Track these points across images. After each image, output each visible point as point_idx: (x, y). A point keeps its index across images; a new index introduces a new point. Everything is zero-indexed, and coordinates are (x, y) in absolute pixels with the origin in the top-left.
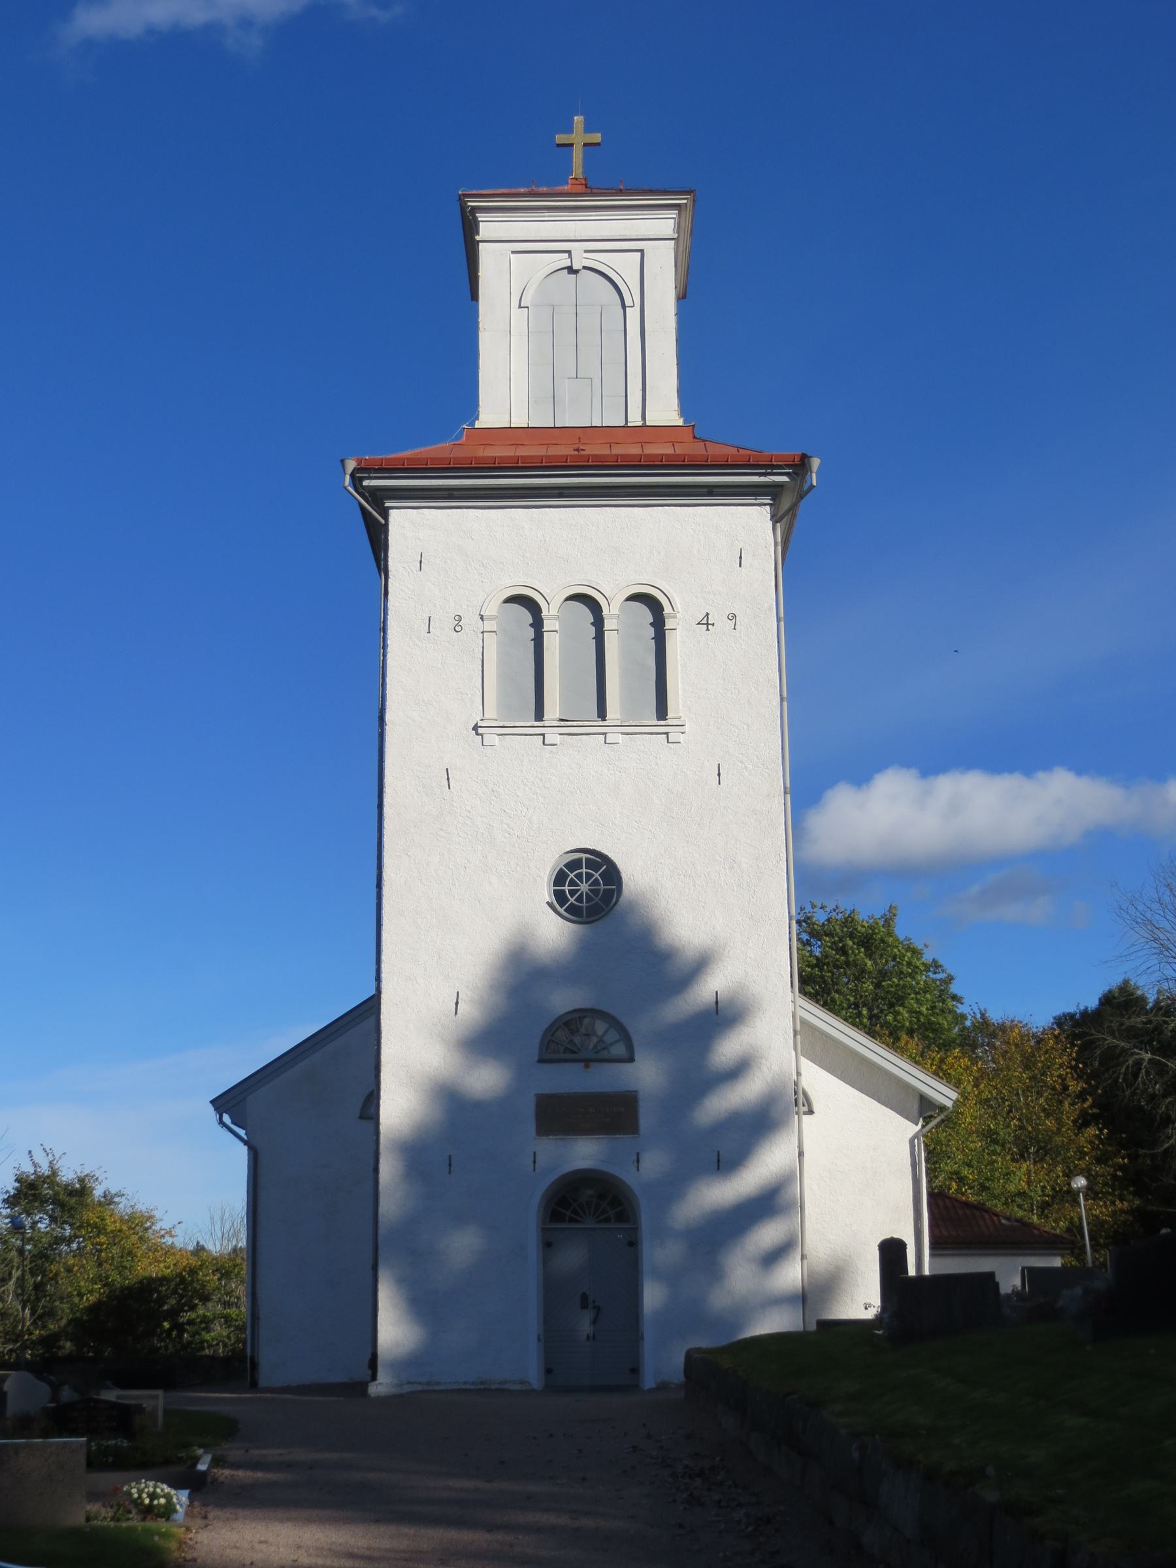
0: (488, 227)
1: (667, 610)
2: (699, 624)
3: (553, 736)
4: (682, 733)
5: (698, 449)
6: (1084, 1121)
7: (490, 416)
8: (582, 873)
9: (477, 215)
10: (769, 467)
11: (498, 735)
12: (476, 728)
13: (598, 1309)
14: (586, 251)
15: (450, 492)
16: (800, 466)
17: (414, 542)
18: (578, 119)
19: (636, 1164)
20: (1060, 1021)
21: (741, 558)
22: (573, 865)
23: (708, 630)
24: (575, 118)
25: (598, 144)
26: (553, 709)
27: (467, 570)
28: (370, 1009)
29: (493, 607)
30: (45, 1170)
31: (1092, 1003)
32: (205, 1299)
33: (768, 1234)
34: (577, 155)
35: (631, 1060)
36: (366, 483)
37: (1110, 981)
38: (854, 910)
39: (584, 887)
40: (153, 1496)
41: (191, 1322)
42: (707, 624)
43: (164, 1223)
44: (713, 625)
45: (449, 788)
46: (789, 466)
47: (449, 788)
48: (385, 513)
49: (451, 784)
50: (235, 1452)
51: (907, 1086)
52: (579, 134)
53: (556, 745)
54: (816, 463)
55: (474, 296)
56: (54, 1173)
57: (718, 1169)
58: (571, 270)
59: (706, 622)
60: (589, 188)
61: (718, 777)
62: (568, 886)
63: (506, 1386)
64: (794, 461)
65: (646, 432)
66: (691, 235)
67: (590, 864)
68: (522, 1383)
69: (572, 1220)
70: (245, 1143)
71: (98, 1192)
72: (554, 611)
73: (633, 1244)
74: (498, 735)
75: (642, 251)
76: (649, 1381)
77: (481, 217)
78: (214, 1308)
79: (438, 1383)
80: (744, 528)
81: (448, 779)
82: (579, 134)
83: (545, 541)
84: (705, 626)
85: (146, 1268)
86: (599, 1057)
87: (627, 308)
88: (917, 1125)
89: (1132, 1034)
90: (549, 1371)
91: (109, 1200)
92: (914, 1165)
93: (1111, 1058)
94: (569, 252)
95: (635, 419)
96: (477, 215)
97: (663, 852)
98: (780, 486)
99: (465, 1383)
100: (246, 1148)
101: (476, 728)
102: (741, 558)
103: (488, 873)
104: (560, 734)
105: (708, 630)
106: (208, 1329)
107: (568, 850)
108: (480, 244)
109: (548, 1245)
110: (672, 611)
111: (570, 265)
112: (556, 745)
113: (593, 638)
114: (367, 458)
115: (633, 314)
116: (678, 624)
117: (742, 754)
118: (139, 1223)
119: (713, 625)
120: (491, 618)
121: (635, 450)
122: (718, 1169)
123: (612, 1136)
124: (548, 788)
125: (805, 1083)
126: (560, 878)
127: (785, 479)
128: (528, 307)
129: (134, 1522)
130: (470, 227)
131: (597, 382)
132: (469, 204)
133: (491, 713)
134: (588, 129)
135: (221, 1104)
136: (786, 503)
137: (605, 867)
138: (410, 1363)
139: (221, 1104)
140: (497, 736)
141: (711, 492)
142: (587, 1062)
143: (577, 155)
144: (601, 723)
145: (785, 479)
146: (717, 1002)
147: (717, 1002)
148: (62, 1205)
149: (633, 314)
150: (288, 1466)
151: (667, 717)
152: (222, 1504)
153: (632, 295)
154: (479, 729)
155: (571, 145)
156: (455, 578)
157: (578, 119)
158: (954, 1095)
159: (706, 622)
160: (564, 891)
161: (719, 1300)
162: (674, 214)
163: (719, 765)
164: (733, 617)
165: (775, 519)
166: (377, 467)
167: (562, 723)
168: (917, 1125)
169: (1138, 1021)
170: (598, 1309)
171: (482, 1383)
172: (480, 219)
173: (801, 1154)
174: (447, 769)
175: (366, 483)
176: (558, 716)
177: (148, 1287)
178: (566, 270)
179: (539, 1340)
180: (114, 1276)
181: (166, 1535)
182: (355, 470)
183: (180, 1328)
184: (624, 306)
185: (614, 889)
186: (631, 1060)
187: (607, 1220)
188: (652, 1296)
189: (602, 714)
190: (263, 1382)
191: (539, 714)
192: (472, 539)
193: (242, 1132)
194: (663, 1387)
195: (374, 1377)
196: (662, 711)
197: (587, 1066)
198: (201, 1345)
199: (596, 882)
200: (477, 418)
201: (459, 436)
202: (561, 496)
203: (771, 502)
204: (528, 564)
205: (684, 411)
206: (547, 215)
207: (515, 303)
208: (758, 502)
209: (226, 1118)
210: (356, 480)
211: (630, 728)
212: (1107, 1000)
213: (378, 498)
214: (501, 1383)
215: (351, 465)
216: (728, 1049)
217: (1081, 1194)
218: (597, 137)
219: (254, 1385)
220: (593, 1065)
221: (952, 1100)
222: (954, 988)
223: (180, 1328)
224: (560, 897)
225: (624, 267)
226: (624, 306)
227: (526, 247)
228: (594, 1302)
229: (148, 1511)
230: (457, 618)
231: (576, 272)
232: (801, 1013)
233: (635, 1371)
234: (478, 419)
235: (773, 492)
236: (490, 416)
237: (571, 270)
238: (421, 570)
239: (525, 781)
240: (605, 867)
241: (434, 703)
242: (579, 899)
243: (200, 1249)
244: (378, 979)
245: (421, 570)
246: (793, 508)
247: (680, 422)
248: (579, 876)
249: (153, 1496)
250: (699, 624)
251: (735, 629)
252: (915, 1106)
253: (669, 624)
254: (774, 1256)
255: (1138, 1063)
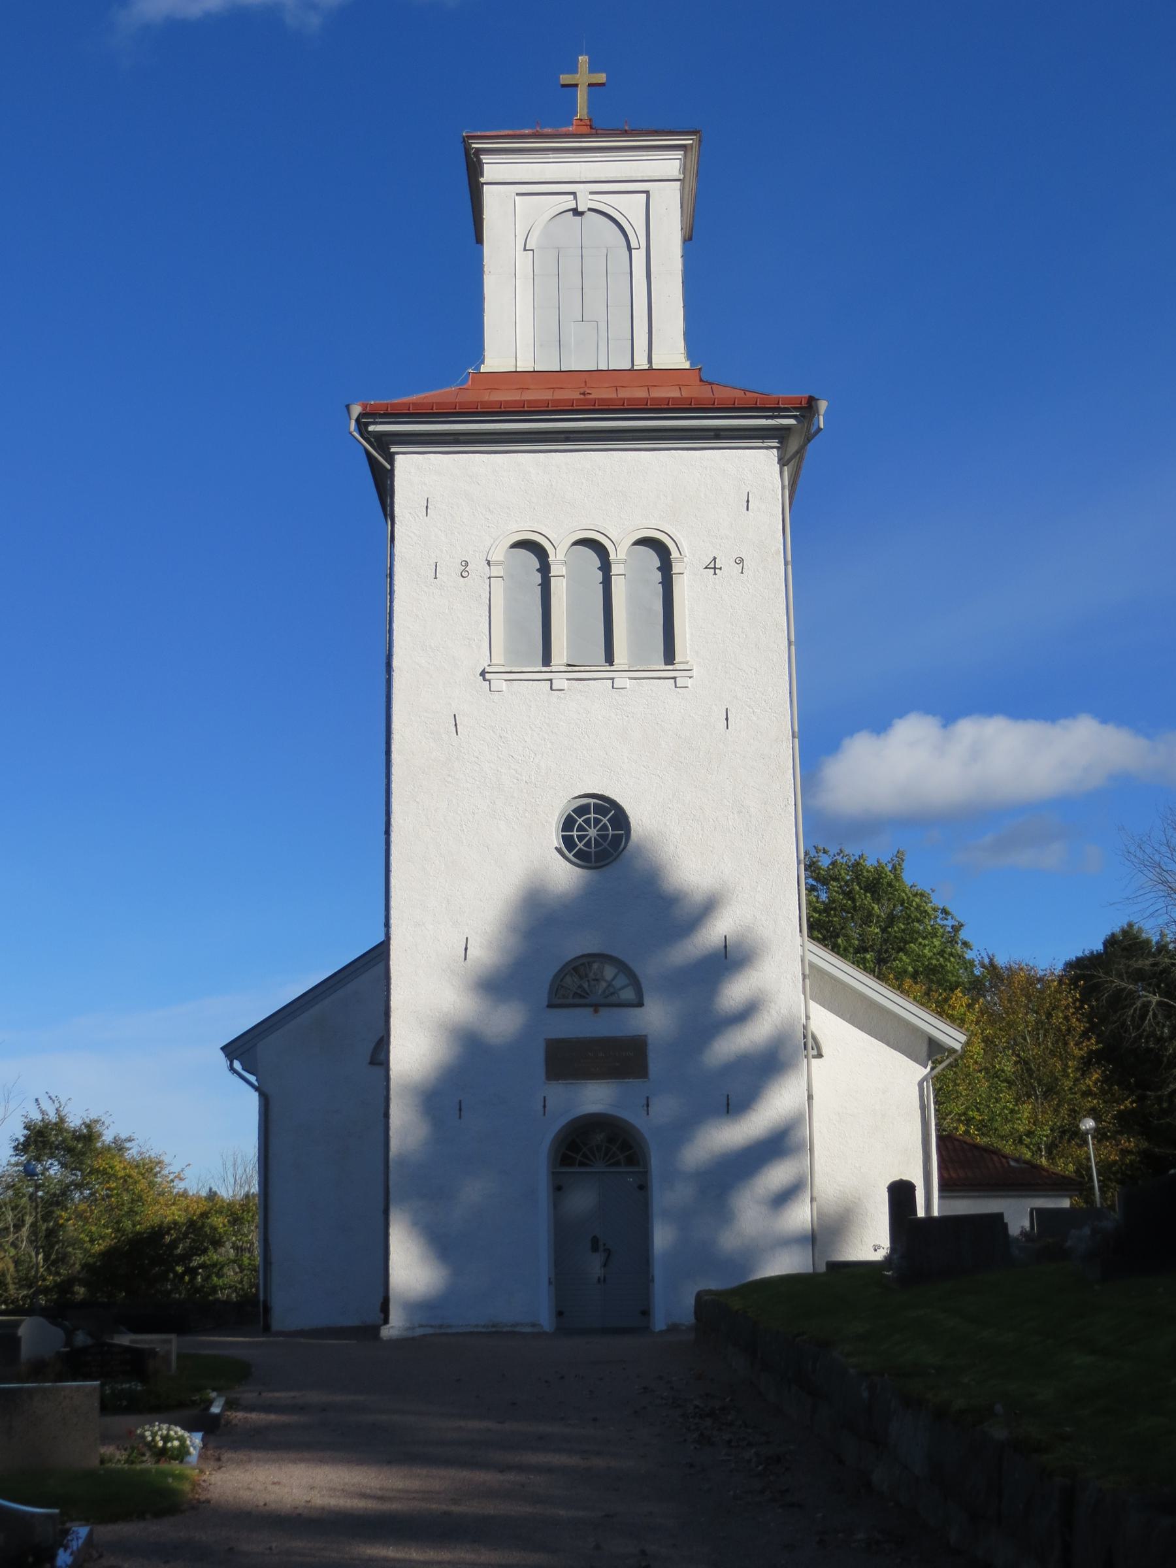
0: (493, 169)
1: (674, 554)
2: (706, 568)
3: (560, 682)
4: (690, 678)
5: (704, 393)
6: (1086, 1065)
7: (495, 360)
8: (590, 818)
9: (481, 157)
10: (776, 410)
11: (506, 680)
12: (483, 674)
13: (609, 1252)
14: (591, 193)
15: (456, 437)
16: (807, 409)
17: (420, 488)
18: (583, 59)
19: (645, 1108)
20: (1069, 965)
21: (748, 501)
22: (582, 810)
23: (715, 574)
24: (580, 58)
25: (603, 85)
26: (560, 654)
27: (474, 515)
28: (379, 955)
29: (499, 553)
30: (53, 1117)
31: (1099, 947)
32: (217, 1243)
33: (777, 1175)
34: (582, 95)
35: (640, 1004)
36: (371, 428)
37: (1113, 925)
38: (862, 854)
39: (592, 832)
40: (166, 1439)
41: (203, 1266)
42: (715, 568)
43: (173, 1166)
44: (720, 569)
45: (457, 734)
46: (796, 409)
47: (457, 734)
48: (391, 459)
49: (458, 730)
50: (248, 1395)
51: (916, 1030)
52: (583, 74)
53: (563, 690)
54: (823, 406)
55: (479, 239)
56: (62, 1120)
57: (725, 937)
58: (576, 212)
59: (713, 567)
60: (594, 129)
61: (725, 722)
62: (577, 832)
63: (517, 1329)
64: (801, 404)
65: (652, 374)
66: (697, 176)
67: (599, 809)
68: (534, 1325)
69: (582, 1164)
70: (256, 1089)
71: (108, 1137)
72: (561, 555)
73: (643, 1187)
74: (506, 680)
75: (647, 192)
76: (659, 1323)
77: (485, 159)
78: (228, 1251)
79: (449, 1326)
80: (751, 471)
81: (456, 725)
82: (583, 74)
83: (552, 485)
84: (713, 570)
85: (155, 1214)
86: (610, 1002)
87: (633, 251)
88: (926, 1067)
89: (1139, 976)
90: (560, 1314)
91: (119, 1146)
92: (923, 1108)
93: (1119, 1000)
94: (574, 194)
95: (641, 363)
96: (481, 157)
97: (671, 797)
98: (787, 429)
99: (477, 1326)
100: (256, 1094)
101: (483, 674)
102: (748, 501)
103: (496, 818)
104: (568, 679)
105: (715, 574)
106: (220, 1275)
107: (577, 795)
108: (485, 186)
109: (558, 1188)
110: (679, 556)
111: (575, 206)
112: (563, 690)
113: (600, 583)
114: (372, 403)
115: (639, 257)
116: (686, 568)
117: (750, 699)
118: (149, 1168)
119: (720, 569)
120: (498, 563)
121: (641, 393)
122: (725, 937)
123: (621, 1081)
124: (556, 733)
125: (814, 1026)
126: (568, 824)
127: (792, 422)
128: (533, 250)
129: (148, 1463)
130: (474, 169)
131: (603, 326)
132: (473, 146)
133: (498, 658)
134: (593, 69)
135: (232, 1050)
136: (793, 445)
137: (613, 812)
138: (424, 1307)
139: (232, 1050)
140: (504, 682)
141: (717, 435)
142: (596, 1007)
143: (582, 95)
144: (609, 668)
145: (792, 422)
146: (726, 947)
147: (726, 947)
148: (70, 1150)
149: (639, 257)
150: (301, 1409)
151: (675, 662)
152: (235, 1446)
153: (638, 238)
154: (486, 674)
155: (576, 85)
156: (462, 523)
157: (583, 59)
158: (963, 1039)
159: (713, 567)
160: (573, 836)
161: (729, 1241)
162: (679, 154)
163: (727, 709)
164: (740, 561)
165: (782, 462)
166: (382, 412)
167: (570, 669)
168: (926, 1067)
169: (1145, 963)
170: (609, 1252)
171: (493, 1326)
172: (484, 161)
173: (810, 1097)
174: (455, 715)
175: (371, 428)
176: (565, 661)
177: (157, 1233)
178: (571, 212)
179: (550, 1283)
180: (127, 1224)
181: (181, 1477)
182: (361, 415)
183: (193, 1272)
184: (629, 248)
185: (622, 834)
186: (640, 1004)
187: (617, 1164)
188: (662, 1237)
189: (610, 659)
190: (276, 1325)
191: (547, 660)
192: (479, 484)
193: (252, 1079)
194: (673, 1329)
195: (386, 1321)
196: (669, 656)
197: (596, 1011)
198: (214, 1289)
199: (604, 828)
200: (483, 362)
201: (465, 381)
202: (567, 440)
203: (779, 445)
204: (535, 509)
205: (690, 354)
206: (552, 157)
207: (520, 246)
208: (765, 445)
209: (237, 1065)
210: (361, 426)
211: (637, 673)
212: (1111, 942)
213: (384, 443)
214: (512, 1326)
215: (356, 410)
216: (736, 992)
217: (1090, 1136)
218: (601, 78)
219: (267, 1329)
220: (604, 1012)
221: (961, 1043)
222: (963, 935)
223: (193, 1272)
224: (568, 842)
225: (630, 208)
226: (629, 248)
227: (530, 189)
228: (604, 1245)
229: (162, 1454)
230: (463, 563)
231: (581, 214)
232: (810, 957)
233: (646, 1313)
234: (483, 363)
235: (780, 435)
236: (495, 360)
237: (576, 212)
238: (427, 515)
239: (533, 726)
240: (613, 812)
241: (441, 649)
242: (588, 844)
243: (212, 1196)
244: (387, 925)
245: (427, 515)
246: (800, 452)
247: (687, 365)
248: (587, 821)
249: (166, 1439)
250: (706, 568)
251: (742, 573)
252: (924, 1049)
253: (676, 568)
254: (784, 1197)
255: (1146, 1006)
